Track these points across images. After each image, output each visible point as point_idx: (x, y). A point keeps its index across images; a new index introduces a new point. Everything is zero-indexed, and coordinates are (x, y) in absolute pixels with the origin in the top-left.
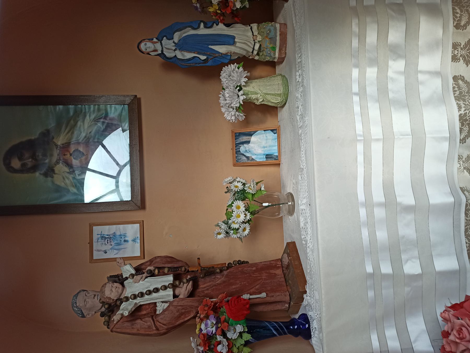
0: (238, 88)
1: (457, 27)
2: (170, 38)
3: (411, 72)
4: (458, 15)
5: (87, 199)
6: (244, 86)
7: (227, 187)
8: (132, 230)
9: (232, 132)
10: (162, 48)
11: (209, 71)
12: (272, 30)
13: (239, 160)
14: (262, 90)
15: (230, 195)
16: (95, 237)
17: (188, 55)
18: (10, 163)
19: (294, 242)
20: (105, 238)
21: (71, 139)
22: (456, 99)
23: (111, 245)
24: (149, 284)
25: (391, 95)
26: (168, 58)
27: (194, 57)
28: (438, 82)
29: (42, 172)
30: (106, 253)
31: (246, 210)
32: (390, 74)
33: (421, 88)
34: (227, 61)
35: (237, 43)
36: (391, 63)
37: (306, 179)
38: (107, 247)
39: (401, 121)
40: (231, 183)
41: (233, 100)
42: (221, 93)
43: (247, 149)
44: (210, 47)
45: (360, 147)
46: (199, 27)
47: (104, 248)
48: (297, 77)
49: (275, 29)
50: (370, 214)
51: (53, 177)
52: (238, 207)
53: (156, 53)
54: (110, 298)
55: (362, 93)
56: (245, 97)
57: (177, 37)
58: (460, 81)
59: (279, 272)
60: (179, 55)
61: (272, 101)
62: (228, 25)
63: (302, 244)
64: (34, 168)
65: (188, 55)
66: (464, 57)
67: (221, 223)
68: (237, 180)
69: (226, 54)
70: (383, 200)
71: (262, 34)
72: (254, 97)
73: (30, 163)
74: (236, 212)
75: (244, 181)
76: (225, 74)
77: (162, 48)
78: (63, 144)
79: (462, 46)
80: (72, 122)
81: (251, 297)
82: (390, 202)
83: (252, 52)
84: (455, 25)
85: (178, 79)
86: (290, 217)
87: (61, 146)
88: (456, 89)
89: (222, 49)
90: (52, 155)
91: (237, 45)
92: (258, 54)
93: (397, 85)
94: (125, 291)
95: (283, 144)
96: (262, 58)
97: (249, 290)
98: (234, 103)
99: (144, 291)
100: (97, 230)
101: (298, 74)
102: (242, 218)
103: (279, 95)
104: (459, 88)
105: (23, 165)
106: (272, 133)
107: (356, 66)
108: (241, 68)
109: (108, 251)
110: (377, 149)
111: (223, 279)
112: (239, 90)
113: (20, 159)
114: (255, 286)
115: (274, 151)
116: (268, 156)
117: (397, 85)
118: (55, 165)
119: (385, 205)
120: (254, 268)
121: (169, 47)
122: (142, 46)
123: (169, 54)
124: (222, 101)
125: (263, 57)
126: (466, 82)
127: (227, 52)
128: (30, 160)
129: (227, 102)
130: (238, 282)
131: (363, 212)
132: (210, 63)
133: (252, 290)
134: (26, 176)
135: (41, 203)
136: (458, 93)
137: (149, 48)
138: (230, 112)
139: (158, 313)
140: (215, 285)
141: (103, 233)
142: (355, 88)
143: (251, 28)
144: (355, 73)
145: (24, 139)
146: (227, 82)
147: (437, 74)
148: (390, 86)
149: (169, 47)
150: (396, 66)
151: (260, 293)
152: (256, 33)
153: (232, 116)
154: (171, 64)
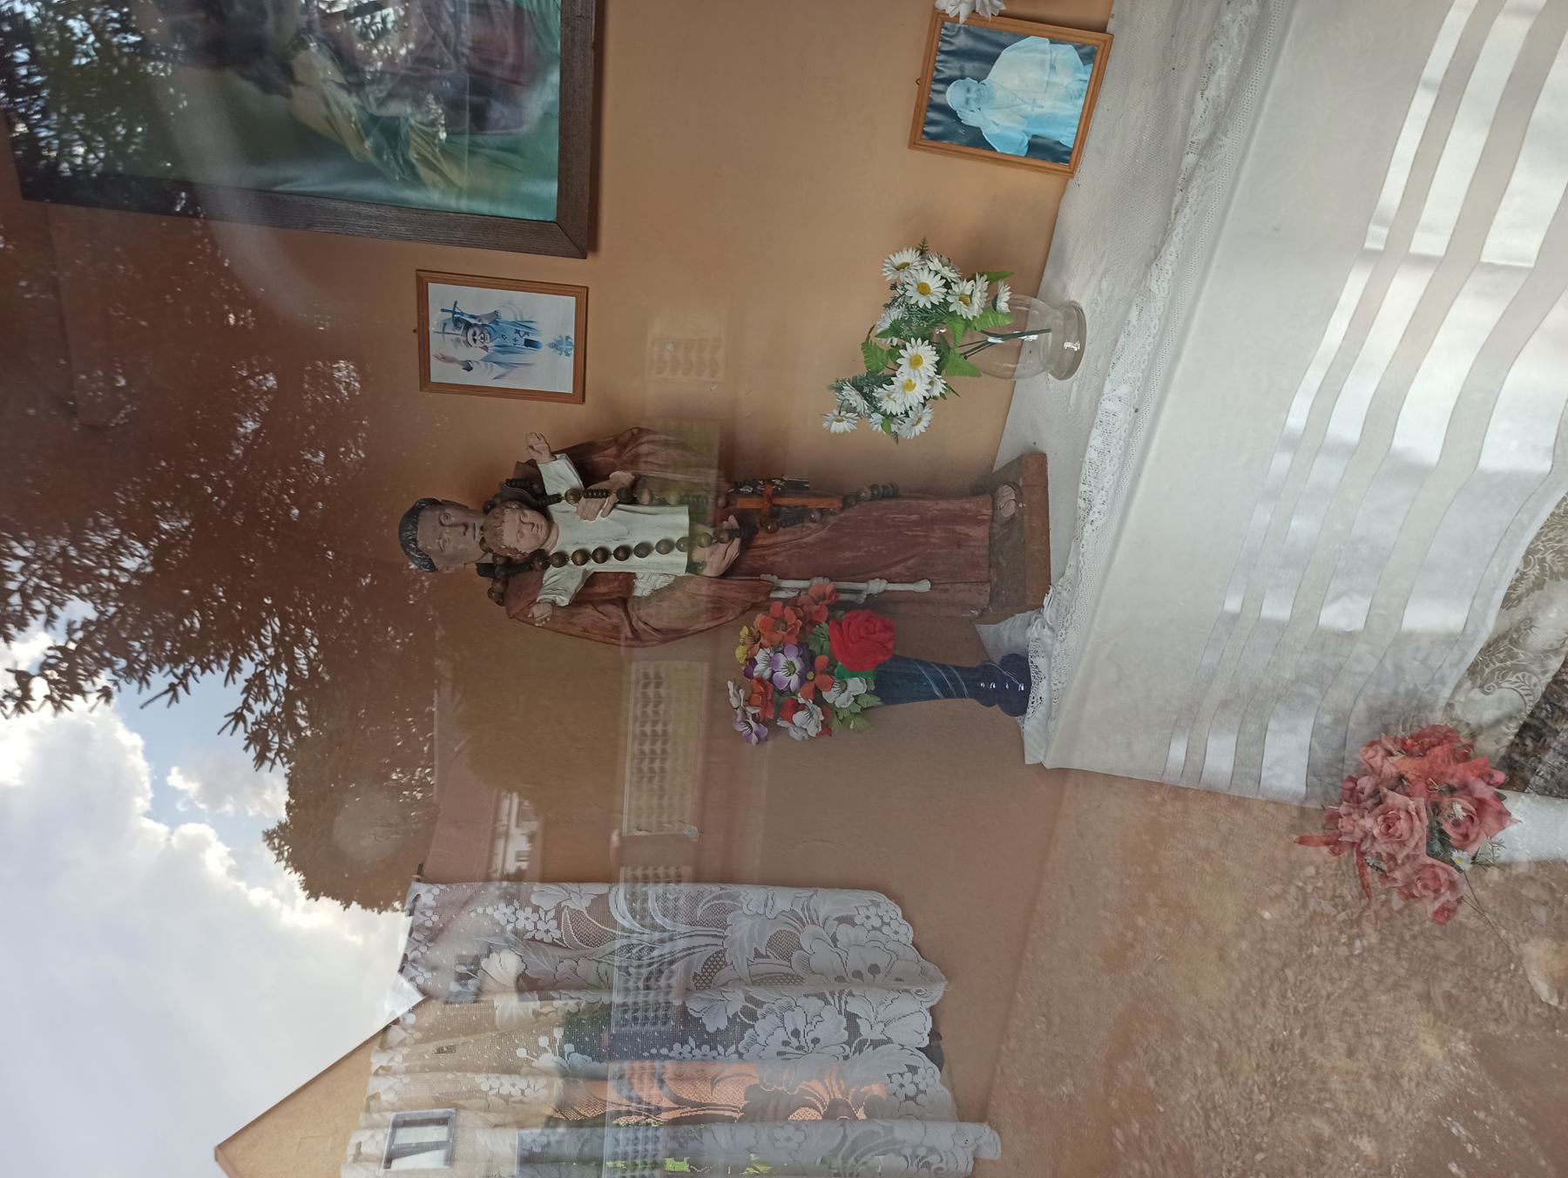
7: (894, 287)
8: (552, 315)
16: (436, 319)
19: (1044, 456)
20: (468, 326)
23: (486, 348)
24: (621, 529)
30: (469, 369)
38: (475, 353)
47: (464, 353)
52: (916, 362)
54: (516, 551)
59: (979, 532)
63: (1075, 507)
81: (891, 587)
94: (554, 532)
97: (888, 567)
99: (612, 547)
100: (441, 296)
109: (474, 365)
111: (823, 533)
114: (906, 560)
115: (1067, 137)
120: (915, 517)
130: (862, 543)
133: (894, 570)
139: (637, 593)
140: (799, 546)
141: (461, 308)
151: (915, 579)
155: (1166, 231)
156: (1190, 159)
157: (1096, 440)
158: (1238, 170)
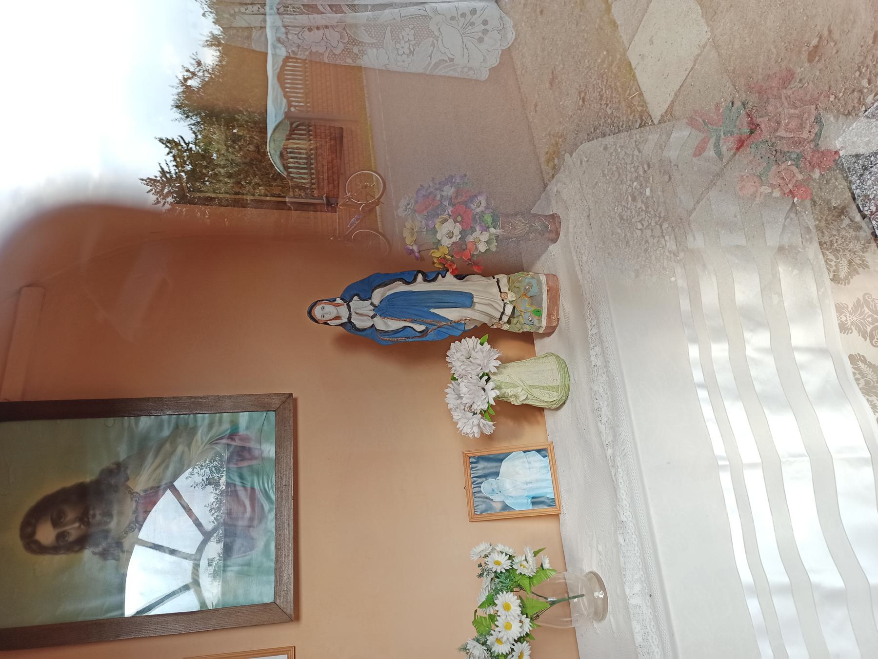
0: (486, 377)
1: (835, 279)
2: (366, 297)
3: (781, 348)
4: (833, 263)
5: (130, 610)
6: (495, 374)
7: (480, 565)
9: (465, 455)
10: (350, 314)
11: (426, 349)
12: (535, 285)
13: (484, 513)
14: (523, 380)
15: (486, 580)
17: (395, 325)
18: (34, 533)
21: (160, 481)
22: (863, 393)
25: (758, 387)
26: (358, 330)
27: (405, 327)
28: (827, 366)
29: (97, 550)
31: (522, 613)
32: (750, 352)
33: (804, 376)
34: (458, 333)
35: (477, 305)
36: (747, 335)
37: (636, 543)
39: (784, 428)
40: (486, 556)
41: (477, 399)
42: (450, 385)
43: (495, 486)
44: (432, 310)
45: (725, 479)
46: (415, 280)
48: (593, 358)
49: (539, 282)
50: (768, 610)
51: (117, 559)
52: (507, 607)
53: (338, 322)
55: (711, 384)
56: (498, 393)
57: (378, 296)
58: (860, 363)
60: (381, 324)
61: (543, 399)
62: (460, 277)
64: (81, 543)
65: (395, 325)
66: (857, 326)
67: (472, 644)
68: (498, 549)
69: (458, 323)
70: (785, 579)
71: (516, 289)
72: (510, 391)
73: (74, 530)
74: (503, 617)
75: (511, 552)
76: (459, 355)
77: (350, 314)
78: (145, 491)
79: (850, 309)
80: (168, 446)
82: (798, 582)
83: (500, 319)
84: (831, 277)
85: (366, 363)
86: (596, 625)
87: (142, 494)
88: (858, 376)
89: (451, 314)
90: (121, 513)
91: (476, 308)
92: (509, 322)
93: (764, 371)
95: (561, 476)
96: (515, 328)
98: (479, 403)
101: (592, 353)
102: (516, 631)
103: (556, 388)
104: (861, 373)
105: (61, 536)
106: (538, 456)
107: (694, 340)
108: (486, 343)
110: (755, 481)
112: (487, 381)
113: (55, 524)
115: (548, 491)
116: (536, 501)
117: (764, 371)
118: (126, 533)
119: (790, 590)
121: (362, 313)
122: (318, 312)
123: (360, 323)
124: (451, 400)
125: (518, 325)
126: (870, 365)
127: (459, 318)
128: (77, 525)
129: (465, 401)
131: (753, 605)
132: (431, 337)
134: (59, 559)
135: (68, 619)
136: (862, 382)
137: (329, 313)
138: (469, 419)
142: (698, 376)
143: (498, 282)
144: (694, 351)
145: (70, 482)
146: (463, 367)
147: (821, 352)
148: (753, 373)
149: (362, 313)
150: (757, 341)
152: (505, 289)
153: (473, 426)
154: (353, 337)
155: (615, 489)
156: (610, 452)
157: (637, 627)
158: (634, 439)
